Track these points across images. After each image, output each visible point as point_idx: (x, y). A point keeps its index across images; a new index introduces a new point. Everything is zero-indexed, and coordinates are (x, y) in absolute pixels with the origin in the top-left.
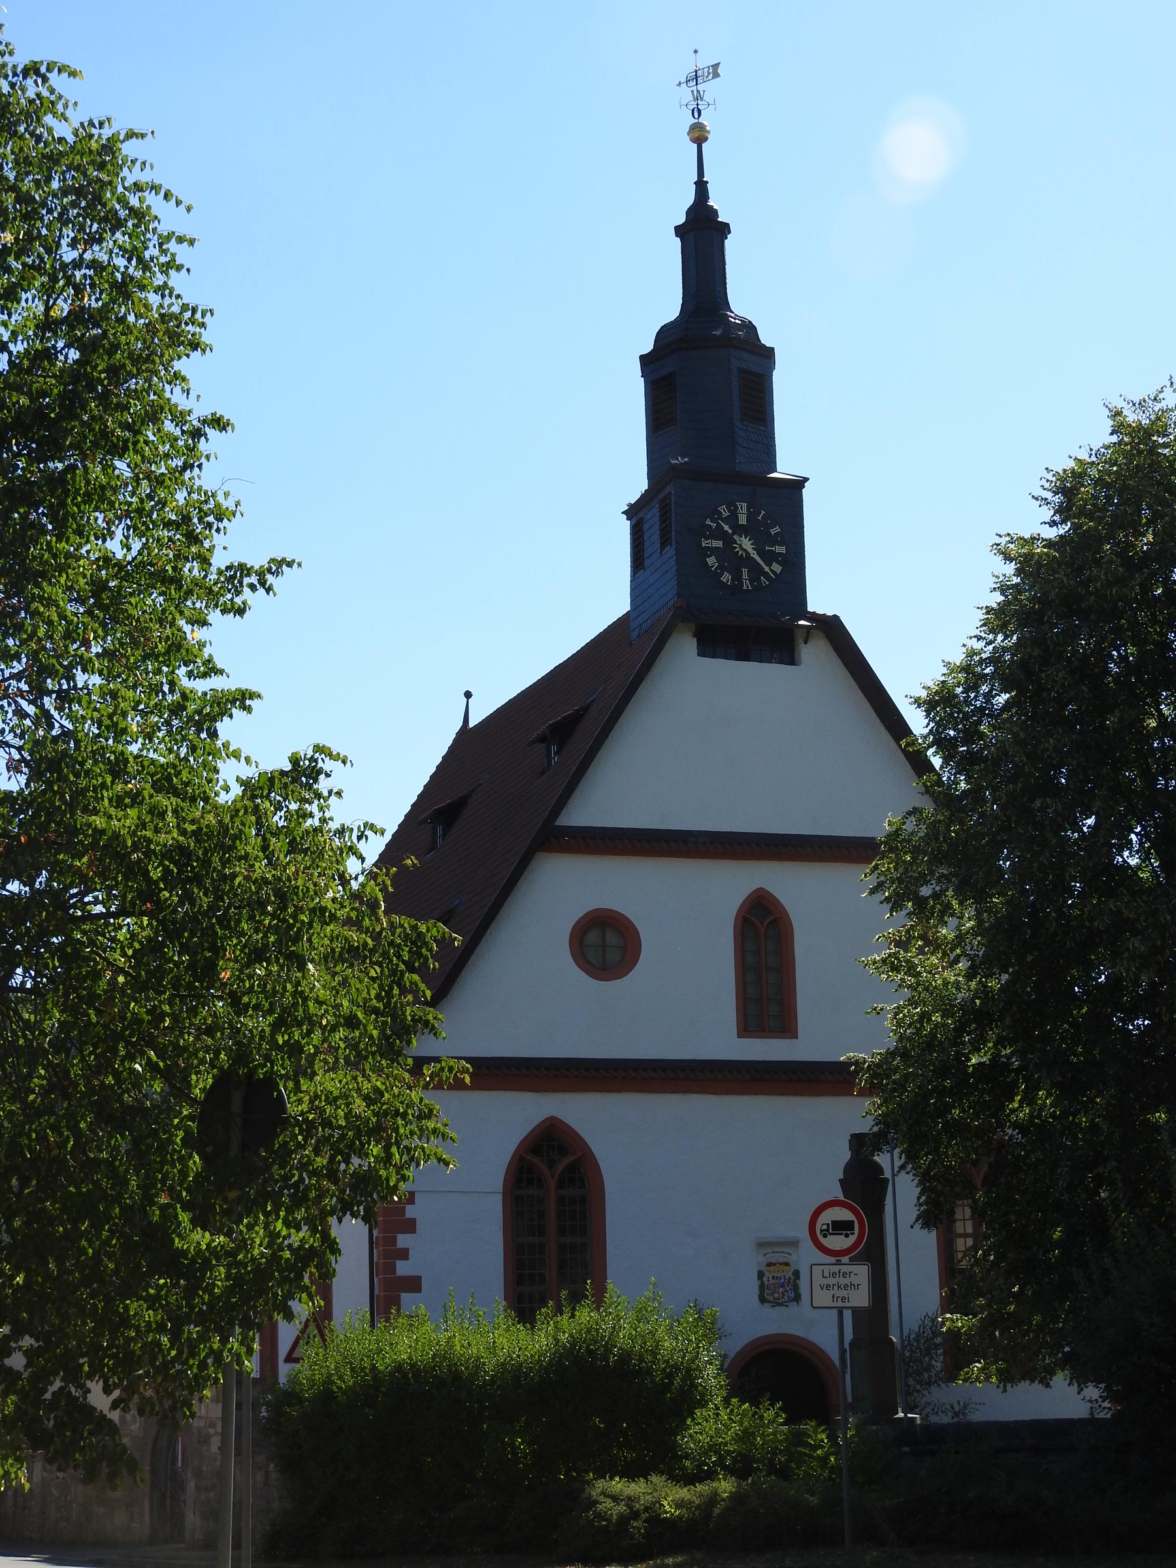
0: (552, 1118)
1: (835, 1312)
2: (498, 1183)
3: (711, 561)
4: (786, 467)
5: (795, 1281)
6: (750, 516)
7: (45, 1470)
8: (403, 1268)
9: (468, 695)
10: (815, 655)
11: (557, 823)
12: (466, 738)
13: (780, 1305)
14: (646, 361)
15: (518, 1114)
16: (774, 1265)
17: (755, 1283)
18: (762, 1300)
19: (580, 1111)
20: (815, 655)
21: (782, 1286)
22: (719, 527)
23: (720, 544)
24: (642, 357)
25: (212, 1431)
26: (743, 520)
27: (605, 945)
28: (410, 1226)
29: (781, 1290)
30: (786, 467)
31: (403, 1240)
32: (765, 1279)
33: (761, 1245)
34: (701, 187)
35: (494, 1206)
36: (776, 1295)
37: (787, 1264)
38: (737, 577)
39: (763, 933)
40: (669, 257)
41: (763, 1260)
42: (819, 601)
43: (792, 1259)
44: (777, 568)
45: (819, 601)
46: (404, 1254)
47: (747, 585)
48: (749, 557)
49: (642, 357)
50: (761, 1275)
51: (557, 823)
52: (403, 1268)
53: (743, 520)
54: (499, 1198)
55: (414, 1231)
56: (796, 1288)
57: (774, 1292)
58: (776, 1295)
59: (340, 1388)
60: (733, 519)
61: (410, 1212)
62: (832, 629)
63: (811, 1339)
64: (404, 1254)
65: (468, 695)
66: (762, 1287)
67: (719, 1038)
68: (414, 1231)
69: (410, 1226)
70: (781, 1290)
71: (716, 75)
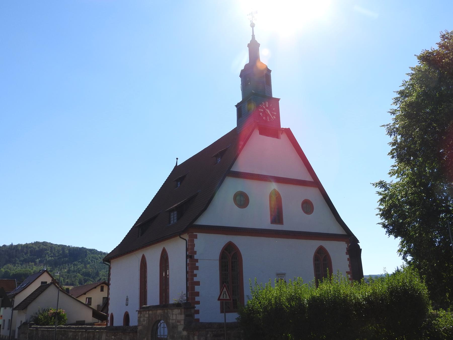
0: (230, 242)
1: (14, 311)
2: (217, 257)
3: (261, 114)
4: (274, 96)
6: (269, 105)
7: (107, 336)
8: (195, 279)
9: (177, 159)
10: (283, 137)
11: (232, 170)
12: (176, 168)
15: (221, 240)
19: (238, 240)
20: (283, 137)
22: (262, 107)
23: (262, 110)
25: (179, 324)
26: (267, 106)
27: (242, 200)
28: (197, 268)
30: (274, 96)
31: (195, 272)
35: (217, 263)
38: (266, 118)
42: (283, 125)
44: (274, 117)
45: (283, 125)
46: (196, 275)
47: (268, 120)
48: (269, 114)
51: (232, 170)
52: (195, 279)
53: (267, 106)
54: (218, 262)
55: (198, 269)
59: (287, 307)
60: (265, 105)
61: (197, 264)
62: (288, 132)
64: (196, 275)
65: (177, 159)
67: (265, 223)
68: (198, 269)
69: (197, 268)
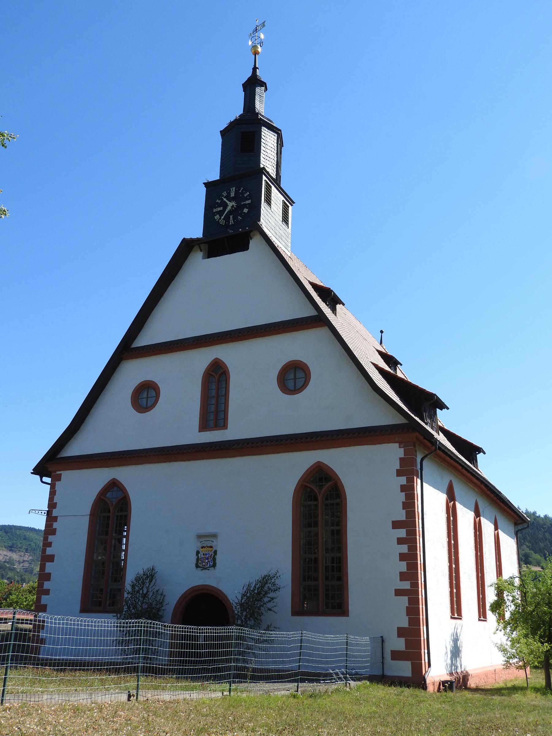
2: (88, 510)
5: (214, 556)
6: (236, 192)
13: (205, 569)
14: (224, 133)
16: (205, 547)
17: (194, 558)
18: (197, 566)
21: (207, 559)
24: (221, 131)
26: (232, 195)
29: (207, 561)
32: (200, 555)
33: (199, 537)
34: (255, 69)
36: (204, 564)
37: (211, 547)
39: (216, 379)
40: (241, 95)
41: (200, 545)
43: (214, 544)
49: (221, 131)
50: (198, 553)
53: (232, 195)
54: (88, 518)
56: (214, 560)
57: (203, 562)
58: (204, 564)
63: (220, 588)
66: (198, 560)
70: (207, 561)
71: (264, 26)
